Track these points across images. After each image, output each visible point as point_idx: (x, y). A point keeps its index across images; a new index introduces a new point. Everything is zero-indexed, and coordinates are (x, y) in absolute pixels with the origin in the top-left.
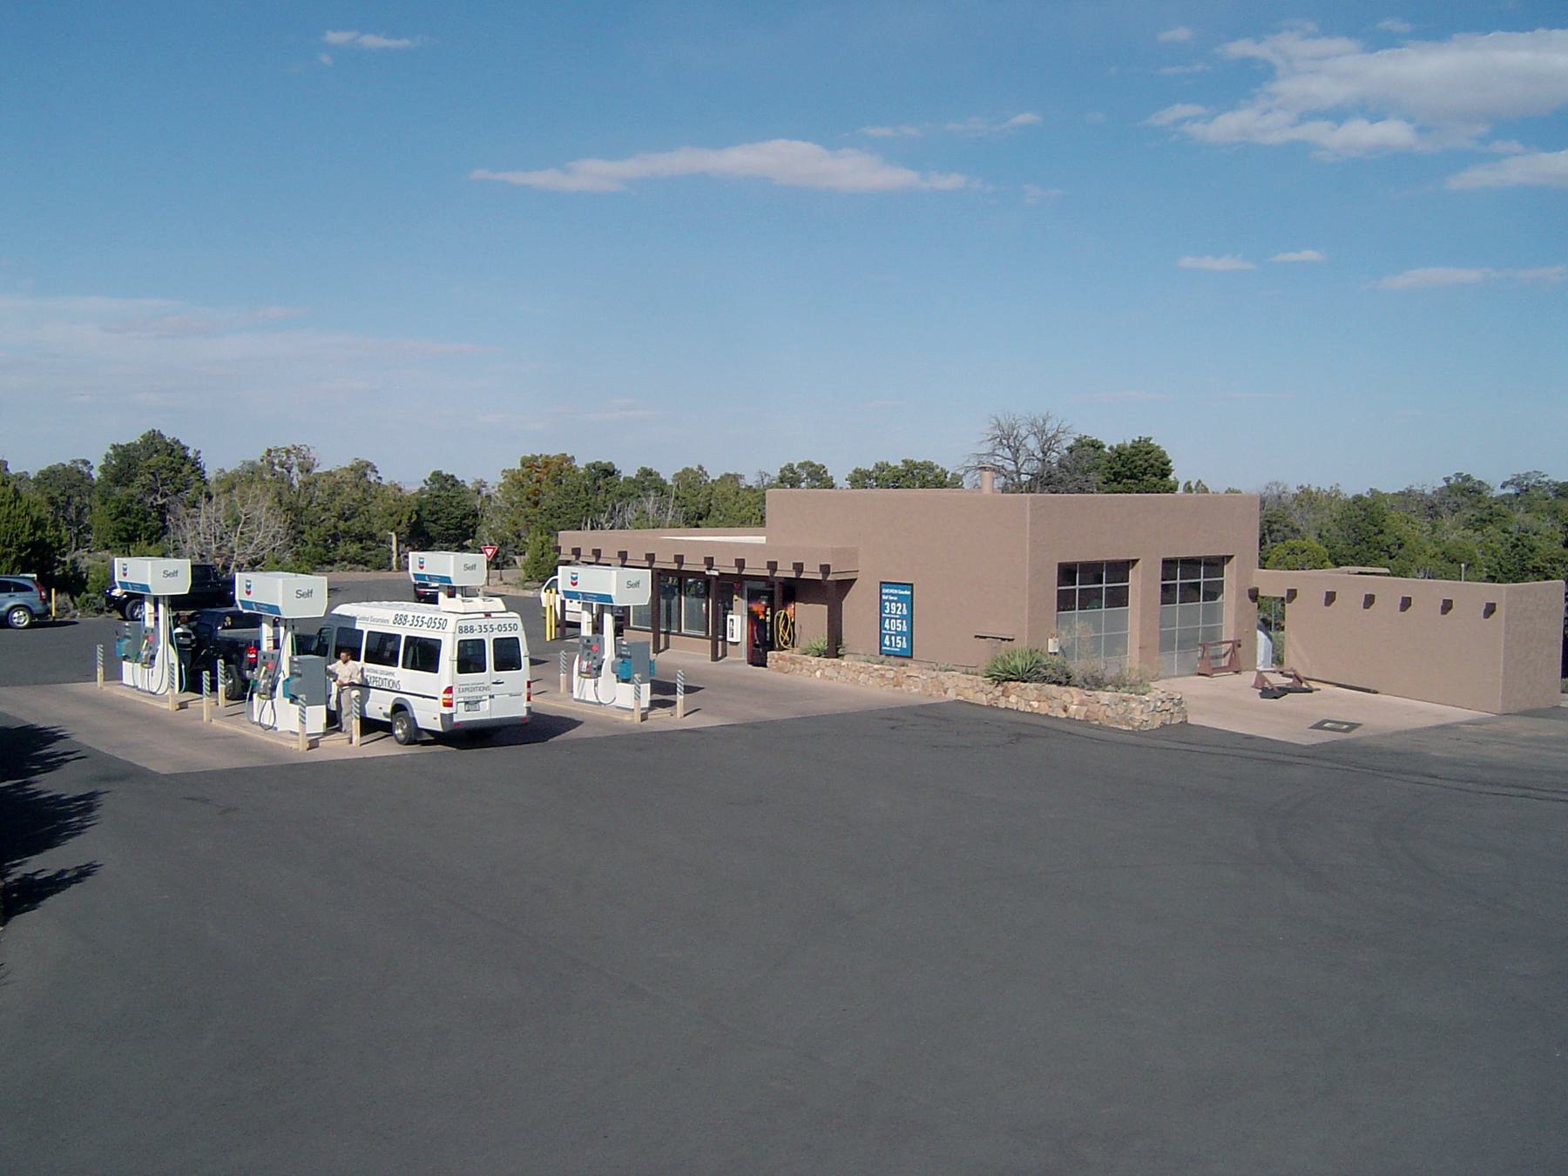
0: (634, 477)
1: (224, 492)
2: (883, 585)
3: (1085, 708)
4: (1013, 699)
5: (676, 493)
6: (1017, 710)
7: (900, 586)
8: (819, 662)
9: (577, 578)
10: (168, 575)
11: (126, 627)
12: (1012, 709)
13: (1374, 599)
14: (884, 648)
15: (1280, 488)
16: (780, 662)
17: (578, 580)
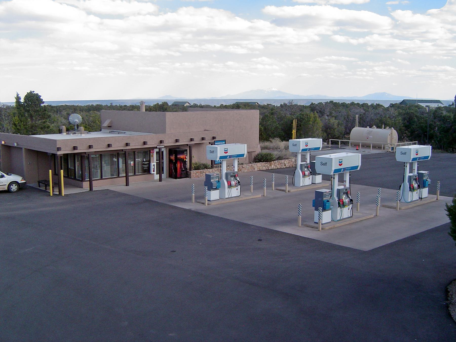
0: (160, 104)
1: (350, 111)
2: (215, 142)
3: (289, 164)
4: (273, 166)
5: (414, 111)
6: (269, 169)
7: (221, 141)
8: (212, 170)
9: (307, 144)
10: (403, 154)
11: (252, 228)
12: (272, 169)
13: (261, 135)
14: (216, 162)
15: (100, 107)
16: (197, 174)
17: (308, 144)
